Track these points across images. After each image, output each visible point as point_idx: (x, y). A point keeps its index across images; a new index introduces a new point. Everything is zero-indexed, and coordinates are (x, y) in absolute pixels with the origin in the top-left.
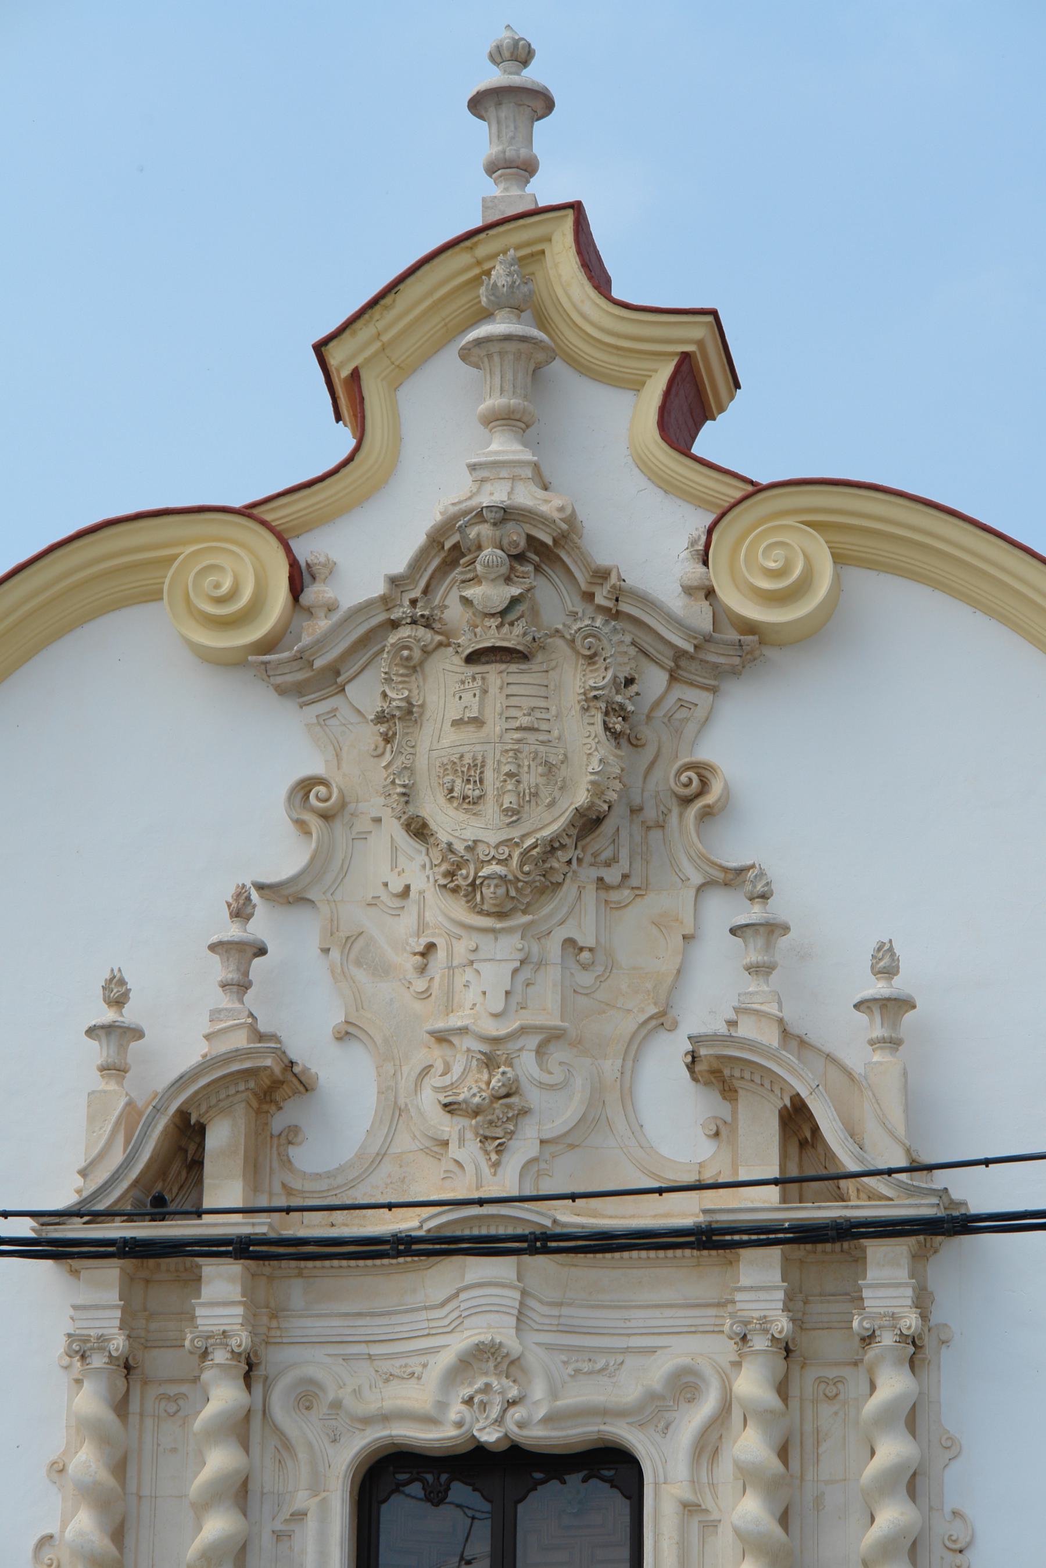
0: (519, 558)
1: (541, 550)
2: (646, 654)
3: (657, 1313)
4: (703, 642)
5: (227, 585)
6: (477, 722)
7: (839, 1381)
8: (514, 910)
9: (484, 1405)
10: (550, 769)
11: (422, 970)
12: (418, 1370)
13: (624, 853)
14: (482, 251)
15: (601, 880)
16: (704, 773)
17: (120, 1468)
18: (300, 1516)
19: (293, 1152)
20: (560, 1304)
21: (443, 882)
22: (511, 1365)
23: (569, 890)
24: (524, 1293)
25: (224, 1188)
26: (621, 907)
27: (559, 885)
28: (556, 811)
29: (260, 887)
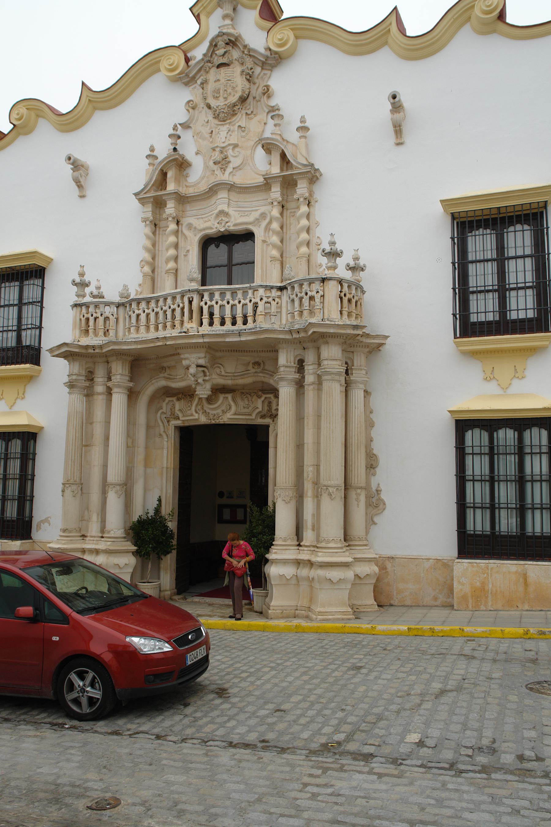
0: (227, 44)
1: (233, 42)
2: (256, 64)
4: (267, 58)
5: (171, 62)
8: (227, 120)
9: (221, 223)
10: (233, 88)
11: (211, 137)
13: (252, 107)
15: (246, 113)
16: (268, 87)
17: (154, 245)
18: (188, 251)
19: (188, 179)
20: (237, 202)
22: (227, 214)
23: (239, 115)
24: (229, 199)
25: (171, 187)
26: (251, 119)
27: (236, 114)
28: (235, 97)
29: (180, 124)
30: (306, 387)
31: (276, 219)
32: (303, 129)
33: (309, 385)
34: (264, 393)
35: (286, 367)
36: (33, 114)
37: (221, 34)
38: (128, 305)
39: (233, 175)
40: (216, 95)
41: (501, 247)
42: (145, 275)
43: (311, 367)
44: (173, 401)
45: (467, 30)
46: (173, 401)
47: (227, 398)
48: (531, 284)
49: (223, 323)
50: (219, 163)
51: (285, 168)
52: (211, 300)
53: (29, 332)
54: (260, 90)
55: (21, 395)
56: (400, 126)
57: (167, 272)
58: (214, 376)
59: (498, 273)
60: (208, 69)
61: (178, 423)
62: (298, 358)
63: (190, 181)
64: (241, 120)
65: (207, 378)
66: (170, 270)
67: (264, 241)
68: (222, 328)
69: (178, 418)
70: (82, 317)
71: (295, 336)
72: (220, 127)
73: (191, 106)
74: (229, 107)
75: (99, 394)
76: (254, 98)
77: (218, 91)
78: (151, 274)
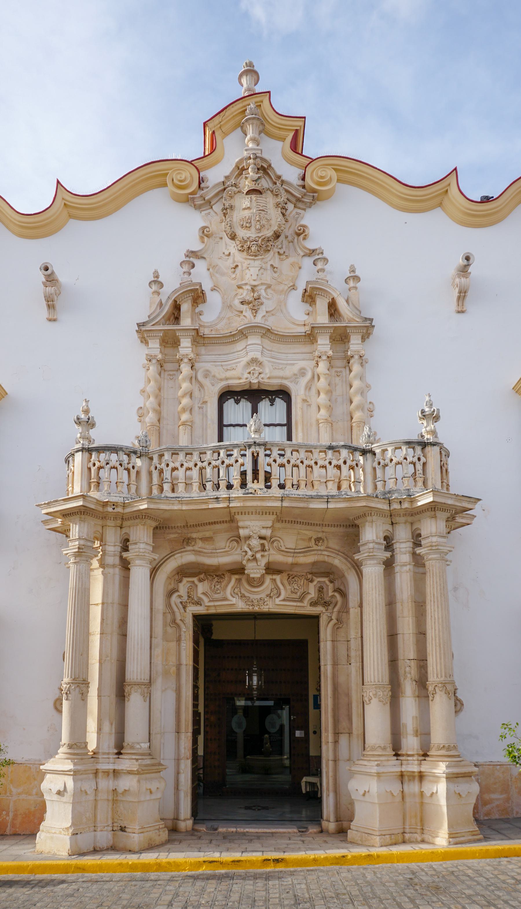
1: (264, 169)
3: (295, 355)
5: (183, 177)
6: (249, 208)
7: (341, 372)
12: (235, 368)
13: (284, 246)
15: (279, 252)
18: (205, 402)
20: (271, 351)
21: (240, 249)
22: (261, 364)
23: (271, 253)
24: (263, 347)
25: (186, 322)
27: (269, 251)
28: (269, 231)
34: (317, 577)
43: (403, 545)
56: (465, 292)
58: (272, 551)
60: (233, 194)
61: (200, 610)
62: (385, 534)
63: (205, 321)
64: (271, 258)
65: (266, 553)
67: (304, 401)
69: (198, 603)
73: (205, 233)
78: (158, 425)
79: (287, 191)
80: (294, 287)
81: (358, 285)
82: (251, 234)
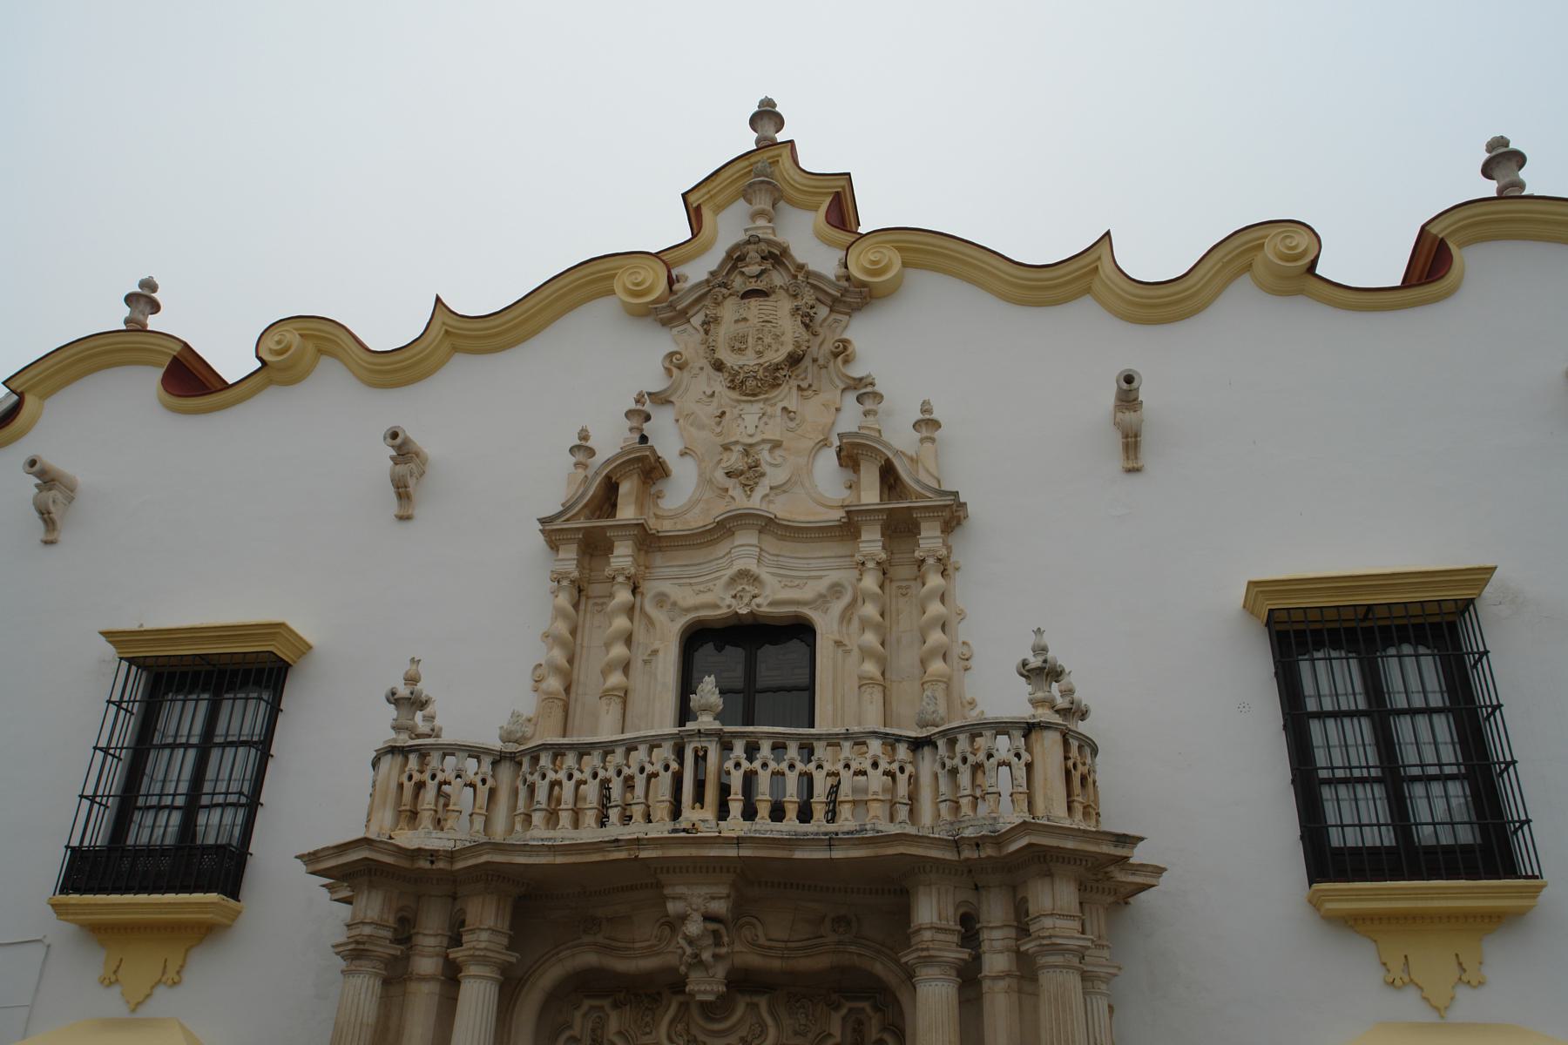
1: (777, 257)
4: (845, 291)
7: (908, 587)
11: (719, 424)
14: (753, 160)
16: (846, 342)
18: (655, 652)
22: (755, 579)
23: (785, 388)
25: (627, 512)
26: (807, 398)
29: (649, 394)
30: (986, 985)
31: (874, 597)
32: (927, 423)
33: (995, 978)
35: (939, 930)
36: (310, 347)
37: (753, 240)
38: (526, 761)
39: (770, 502)
40: (737, 345)
41: (1374, 687)
42: (550, 697)
43: (997, 934)
44: (601, 1008)
45: (1244, 284)
46: (601, 1008)
47: (755, 1006)
48: (1454, 770)
49: (778, 813)
50: (742, 473)
51: (885, 497)
52: (750, 759)
53: (215, 815)
54: (829, 346)
55: (171, 973)
56: (1136, 436)
57: (607, 694)
58: (738, 947)
59: (1377, 744)
62: (961, 910)
64: (787, 396)
65: (723, 950)
66: (614, 689)
67: (838, 643)
68: (778, 826)
70: (404, 779)
71: (967, 853)
72: (743, 405)
73: (675, 363)
74: (766, 369)
75: (423, 979)
76: (815, 360)
77: (743, 339)
78: (563, 696)
79: (814, 287)
80: (825, 443)
81: (937, 435)
82: (749, 360)
